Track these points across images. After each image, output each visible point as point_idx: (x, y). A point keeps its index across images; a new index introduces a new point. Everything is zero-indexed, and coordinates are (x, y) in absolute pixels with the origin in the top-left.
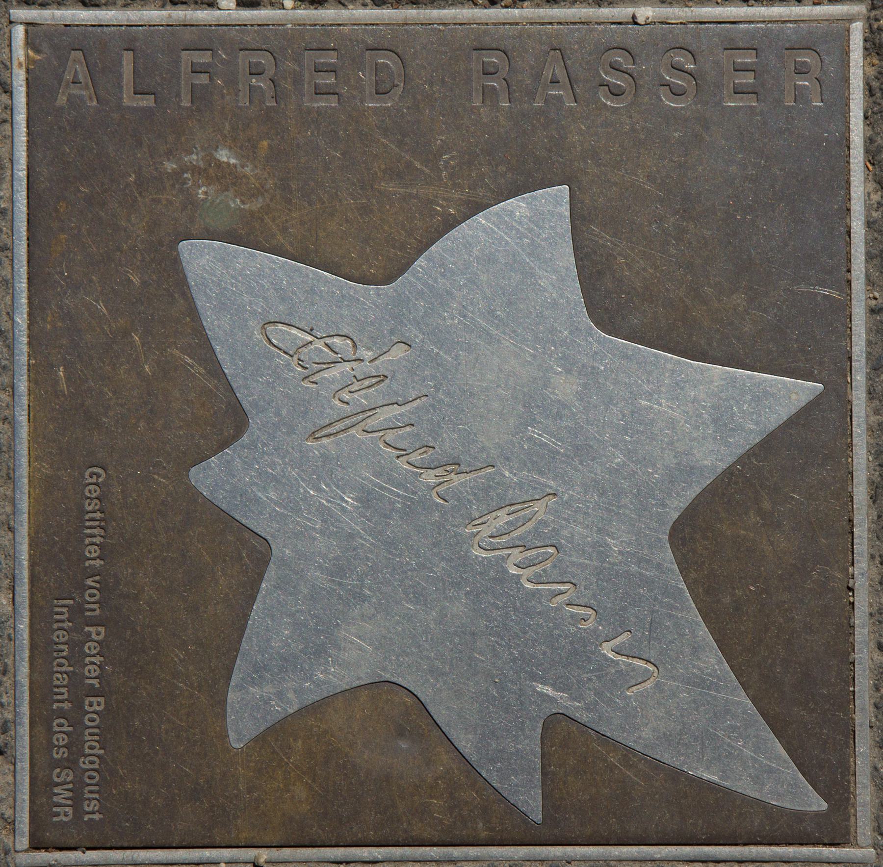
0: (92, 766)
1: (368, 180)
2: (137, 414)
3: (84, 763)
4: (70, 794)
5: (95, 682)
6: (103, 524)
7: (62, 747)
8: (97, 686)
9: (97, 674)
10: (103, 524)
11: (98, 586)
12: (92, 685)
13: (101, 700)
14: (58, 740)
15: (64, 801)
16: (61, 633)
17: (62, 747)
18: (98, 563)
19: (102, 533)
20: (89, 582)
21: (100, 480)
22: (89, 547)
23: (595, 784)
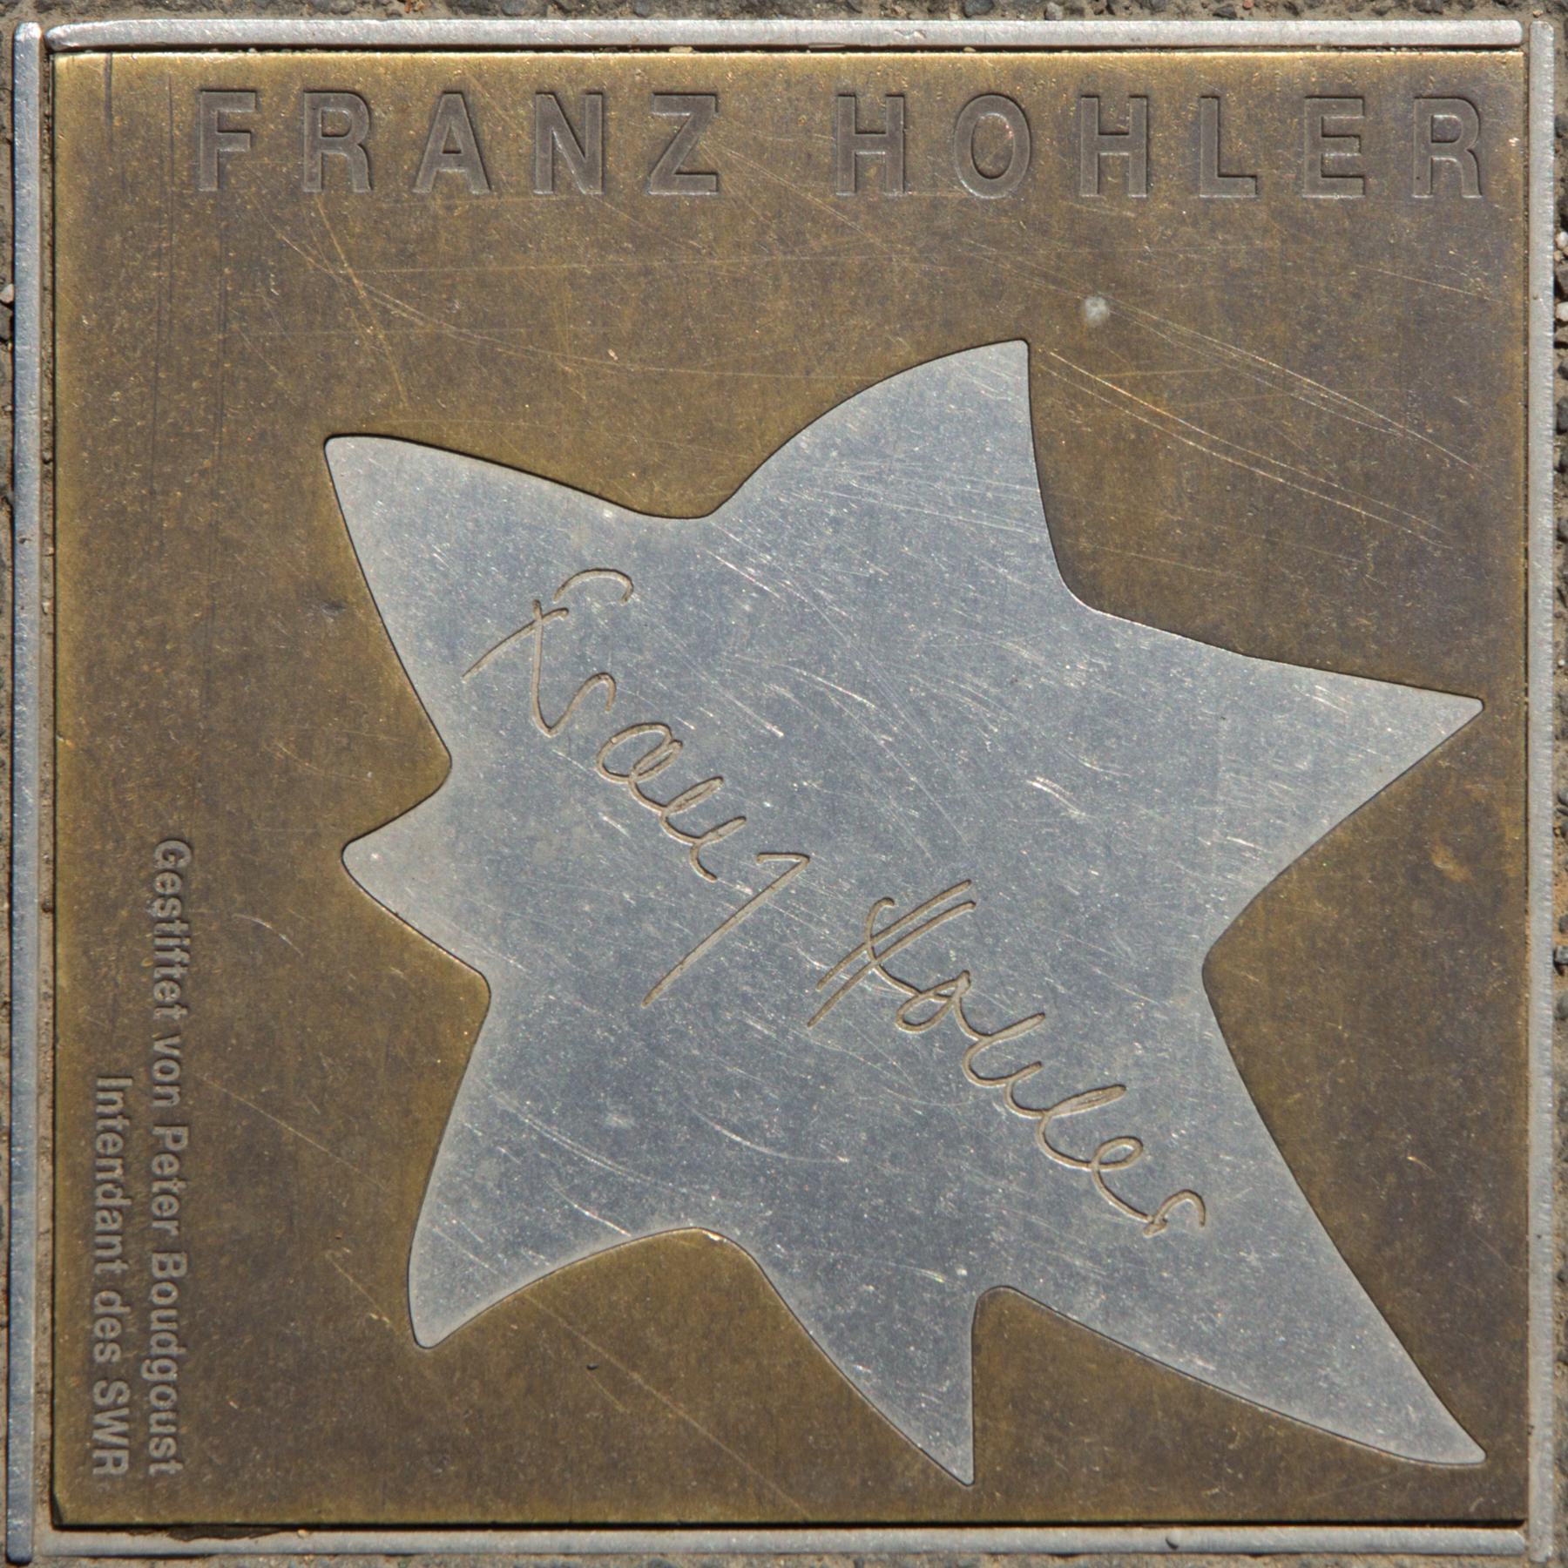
0: (165, 1377)
1: (653, 290)
2: (239, 735)
3: (150, 1371)
4: (123, 1427)
5: (171, 1227)
6: (187, 942)
7: (112, 1341)
8: (175, 1232)
9: (175, 1210)
10: (187, 942)
11: (176, 1053)
12: (167, 1232)
13: (181, 1258)
14: (160, 1207)
15: (115, 1440)
16: (109, 1137)
17: (112, 1341)
18: (177, 1013)
19: (185, 957)
20: (159, 1047)
21: (182, 863)
22: (161, 1199)
23: (1072, 1418)
